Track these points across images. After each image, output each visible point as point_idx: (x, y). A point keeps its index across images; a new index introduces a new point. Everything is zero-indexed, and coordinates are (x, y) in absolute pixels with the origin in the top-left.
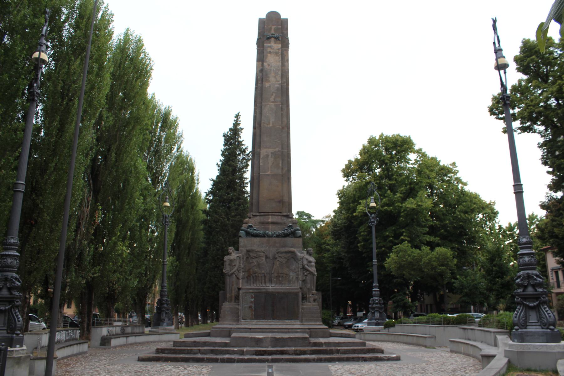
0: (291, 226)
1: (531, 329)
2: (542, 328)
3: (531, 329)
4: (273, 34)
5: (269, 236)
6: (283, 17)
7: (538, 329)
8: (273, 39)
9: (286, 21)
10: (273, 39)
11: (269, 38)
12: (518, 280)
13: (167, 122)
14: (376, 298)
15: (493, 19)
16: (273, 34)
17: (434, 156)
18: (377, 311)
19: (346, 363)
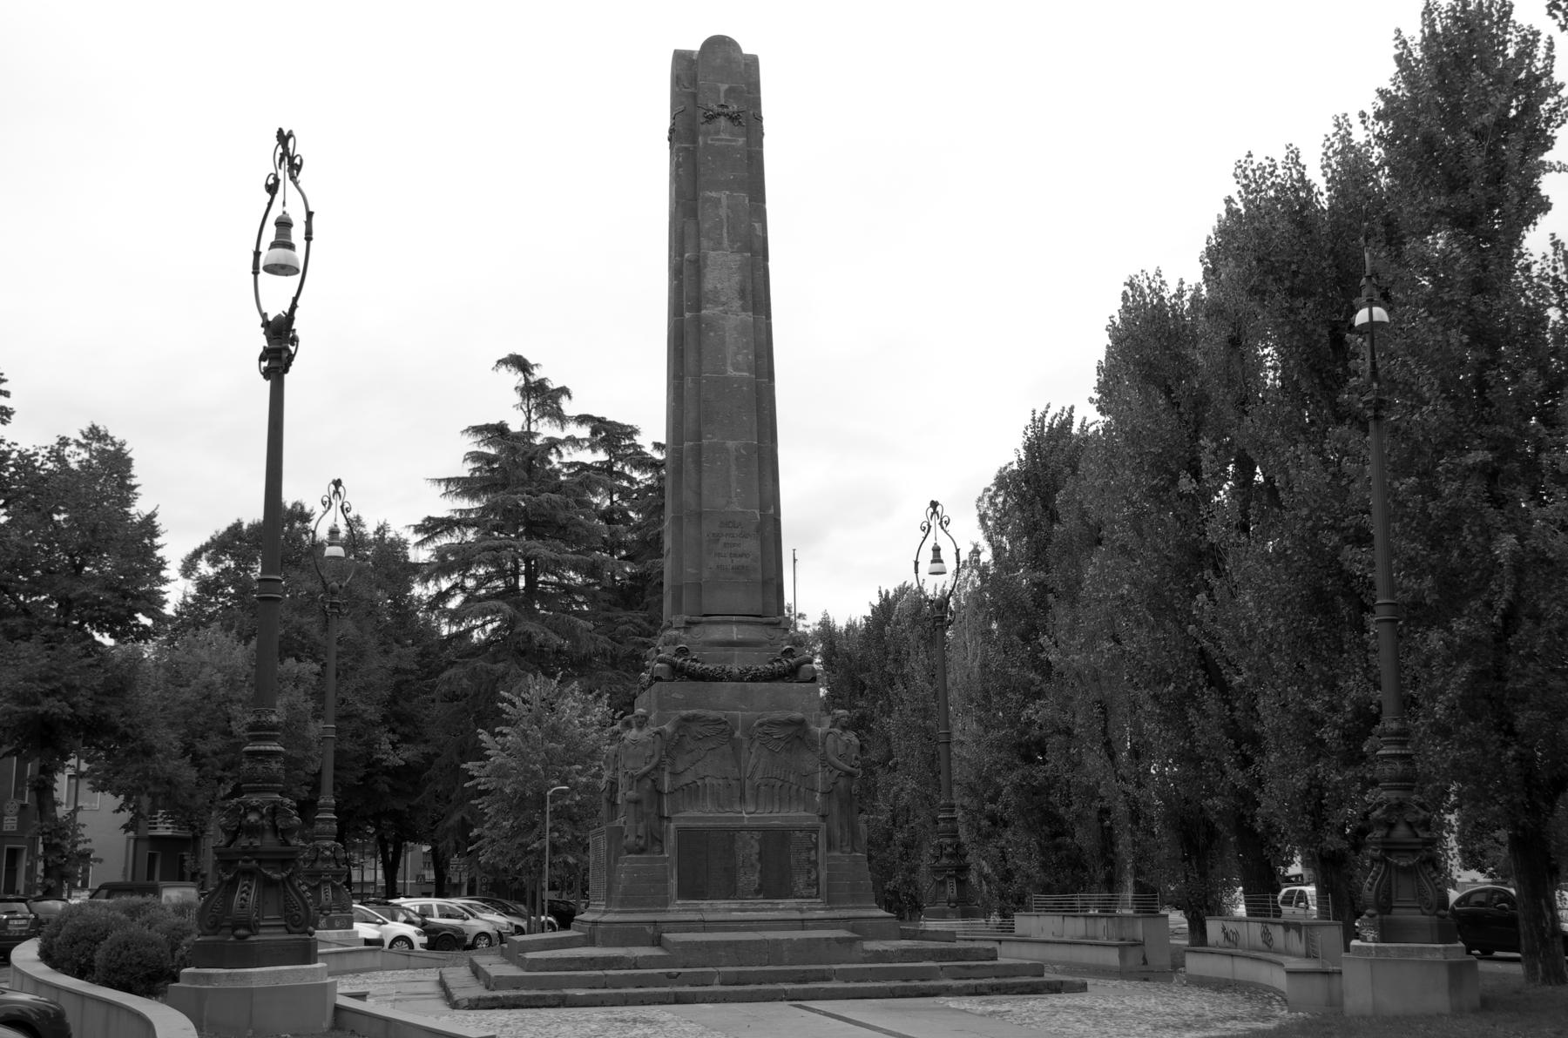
0: (790, 650)
1: (264, 936)
2: (290, 932)
3: (264, 936)
4: (716, 108)
5: (731, 677)
6: (747, 49)
7: (281, 936)
8: (723, 122)
9: (752, 62)
10: (723, 122)
11: (710, 118)
12: (1378, 812)
13: (1113, 330)
14: (328, 844)
15: (280, 131)
16: (716, 108)
17: (994, 473)
18: (249, 874)
19: (1141, 985)
